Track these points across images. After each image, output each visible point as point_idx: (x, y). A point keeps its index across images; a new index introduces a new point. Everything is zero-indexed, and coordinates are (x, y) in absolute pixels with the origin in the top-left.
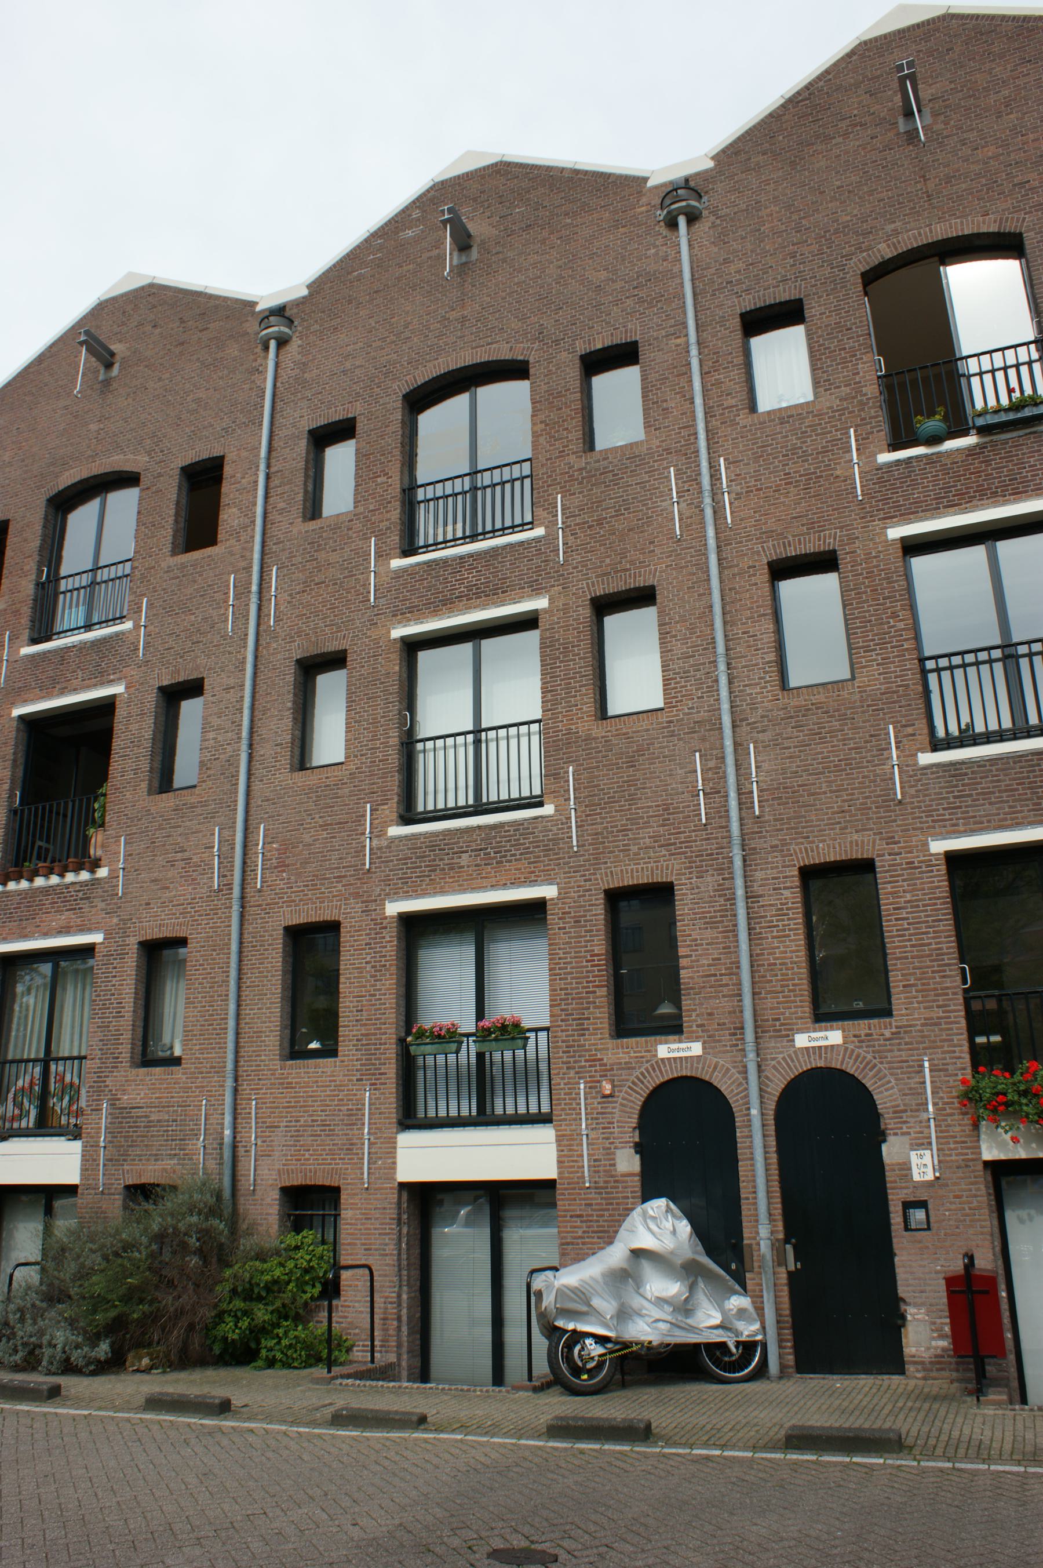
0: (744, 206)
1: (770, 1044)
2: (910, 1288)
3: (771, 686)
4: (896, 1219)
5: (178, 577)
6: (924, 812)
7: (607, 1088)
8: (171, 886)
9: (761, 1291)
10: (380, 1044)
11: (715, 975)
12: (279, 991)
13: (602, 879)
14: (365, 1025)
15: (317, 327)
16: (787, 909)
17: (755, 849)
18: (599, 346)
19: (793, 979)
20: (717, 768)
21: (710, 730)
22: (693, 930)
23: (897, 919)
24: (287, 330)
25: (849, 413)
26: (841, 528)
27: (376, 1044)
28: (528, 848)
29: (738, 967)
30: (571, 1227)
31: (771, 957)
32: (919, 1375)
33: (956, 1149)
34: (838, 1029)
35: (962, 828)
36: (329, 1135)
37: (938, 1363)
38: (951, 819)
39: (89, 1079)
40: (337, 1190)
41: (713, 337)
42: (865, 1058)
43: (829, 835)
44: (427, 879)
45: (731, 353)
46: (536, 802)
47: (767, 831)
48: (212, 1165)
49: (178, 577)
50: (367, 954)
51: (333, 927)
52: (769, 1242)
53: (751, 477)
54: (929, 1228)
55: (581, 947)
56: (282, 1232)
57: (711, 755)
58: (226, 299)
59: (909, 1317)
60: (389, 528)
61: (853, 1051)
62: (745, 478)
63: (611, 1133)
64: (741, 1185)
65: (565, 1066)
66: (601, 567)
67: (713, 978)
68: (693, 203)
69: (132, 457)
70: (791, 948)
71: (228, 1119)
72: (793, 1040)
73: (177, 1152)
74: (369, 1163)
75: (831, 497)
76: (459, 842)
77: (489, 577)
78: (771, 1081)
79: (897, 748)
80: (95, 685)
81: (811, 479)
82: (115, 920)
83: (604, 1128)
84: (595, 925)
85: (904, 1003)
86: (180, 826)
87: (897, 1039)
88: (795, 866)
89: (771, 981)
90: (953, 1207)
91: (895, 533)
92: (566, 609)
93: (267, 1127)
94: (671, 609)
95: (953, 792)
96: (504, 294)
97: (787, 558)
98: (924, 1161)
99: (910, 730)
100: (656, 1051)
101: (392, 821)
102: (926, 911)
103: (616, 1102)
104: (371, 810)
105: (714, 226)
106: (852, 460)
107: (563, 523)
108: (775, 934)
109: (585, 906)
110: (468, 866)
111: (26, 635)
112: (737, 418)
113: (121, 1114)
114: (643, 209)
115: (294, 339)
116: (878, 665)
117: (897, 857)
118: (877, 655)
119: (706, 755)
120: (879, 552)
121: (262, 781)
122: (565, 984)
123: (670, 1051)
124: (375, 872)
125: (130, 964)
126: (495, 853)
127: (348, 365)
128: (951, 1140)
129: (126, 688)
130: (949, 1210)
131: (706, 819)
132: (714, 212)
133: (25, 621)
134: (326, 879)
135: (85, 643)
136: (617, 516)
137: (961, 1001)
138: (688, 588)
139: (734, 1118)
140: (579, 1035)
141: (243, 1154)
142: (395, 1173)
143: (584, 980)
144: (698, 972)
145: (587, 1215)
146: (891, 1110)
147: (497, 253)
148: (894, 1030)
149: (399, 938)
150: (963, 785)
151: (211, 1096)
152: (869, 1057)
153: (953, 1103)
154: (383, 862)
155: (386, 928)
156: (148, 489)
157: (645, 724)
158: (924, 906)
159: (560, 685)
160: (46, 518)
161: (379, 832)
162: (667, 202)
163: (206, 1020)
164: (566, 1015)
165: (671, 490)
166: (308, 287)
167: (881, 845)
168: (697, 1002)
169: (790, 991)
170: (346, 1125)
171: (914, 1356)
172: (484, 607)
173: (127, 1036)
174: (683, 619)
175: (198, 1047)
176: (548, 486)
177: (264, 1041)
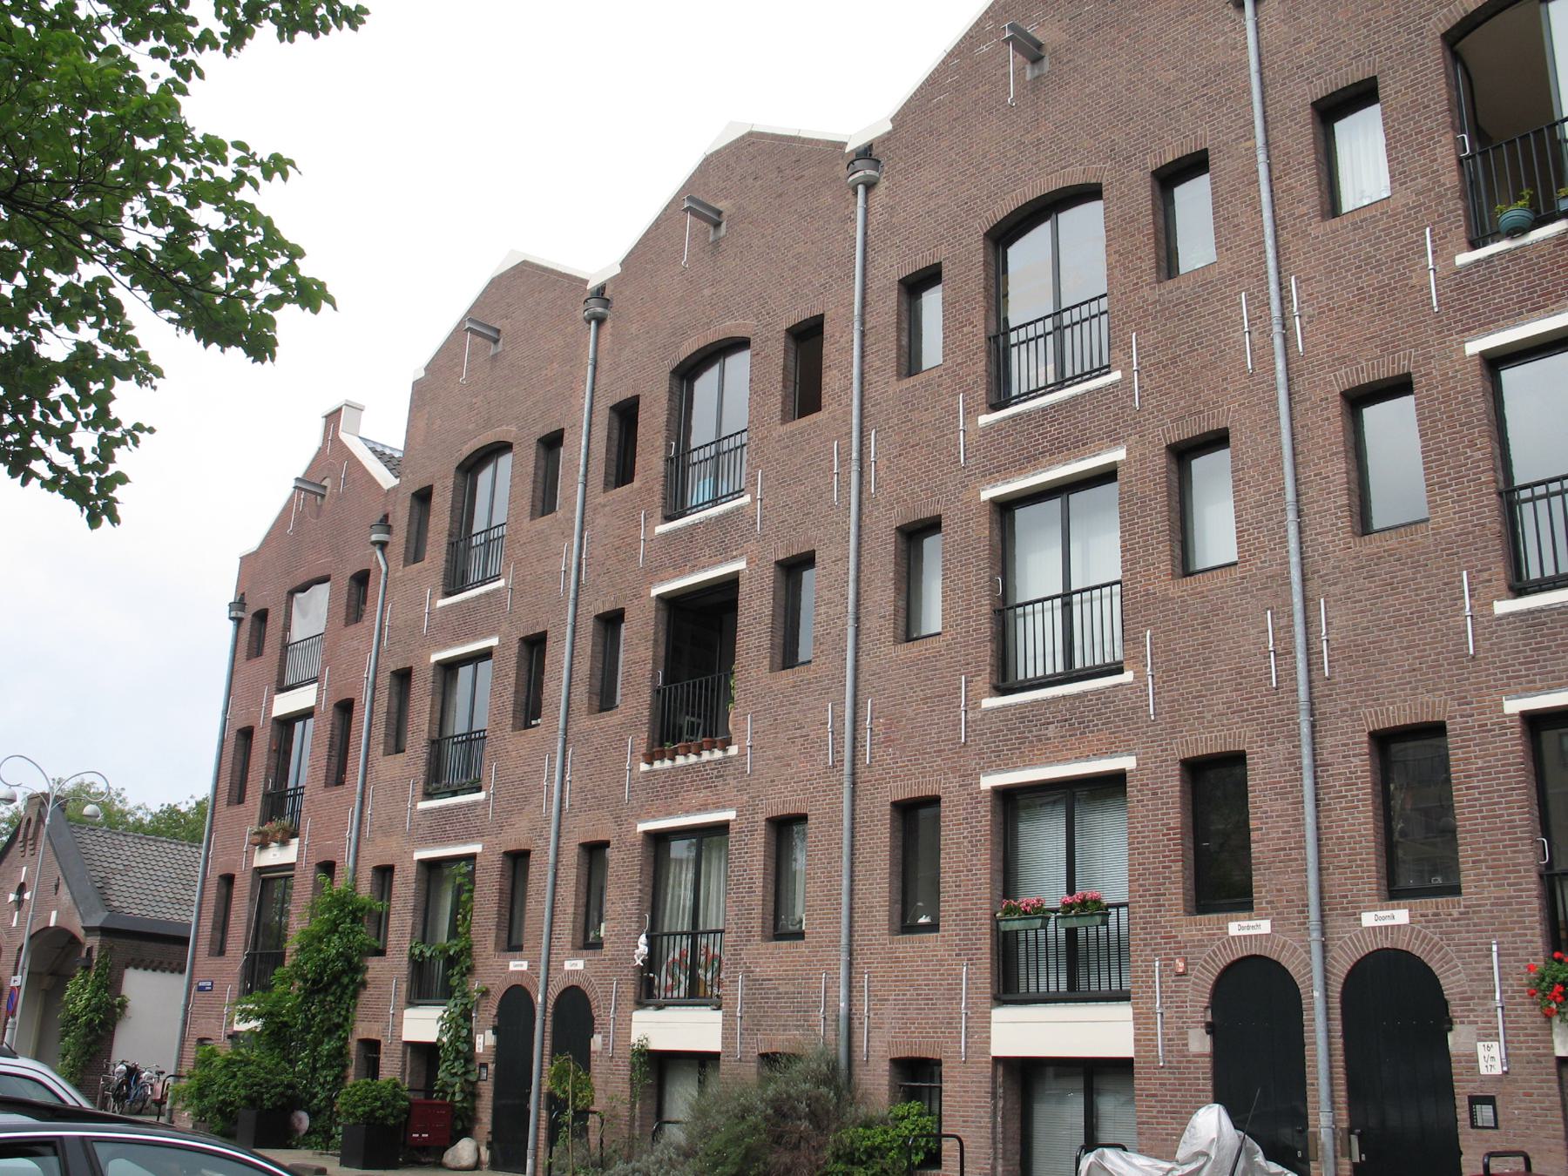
1: (1336, 922)
4: (1463, 1114)
7: (1180, 966)
15: (901, 164)
18: (1170, 159)
24: (873, 173)
39: (728, 950)
46: (1117, 669)
48: (831, 1035)
54: (1496, 1127)
56: (893, 1101)
70: (1358, 821)
71: (843, 992)
77: (1064, 429)
82: (745, 797)
97: (1361, 386)
99: (1485, 575)
111: (659, 513)
113: (753, 982)
123: (1241, 928)
126: (1077, 724)
133: (658, 499)
149: (993, 812)
152: (1436, 938)
157: (1393, 543)
160: (671, 391)
161: (973, 704)
167: (1452, 706)
172: (1066, 461)
173: (758, 910)
174: (1256, 463)
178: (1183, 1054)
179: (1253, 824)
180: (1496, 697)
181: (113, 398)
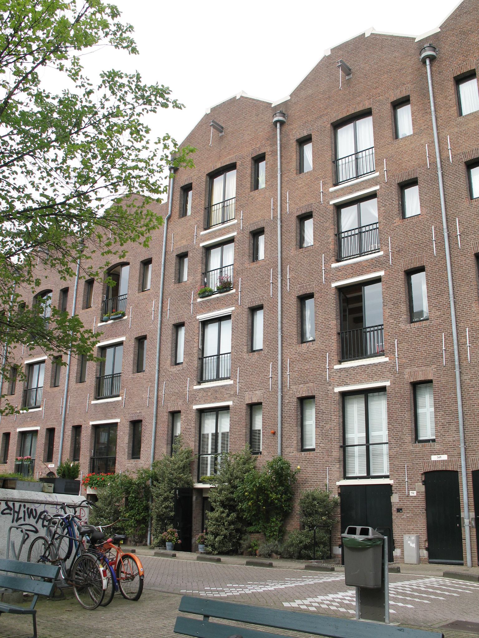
181: (141, 77)
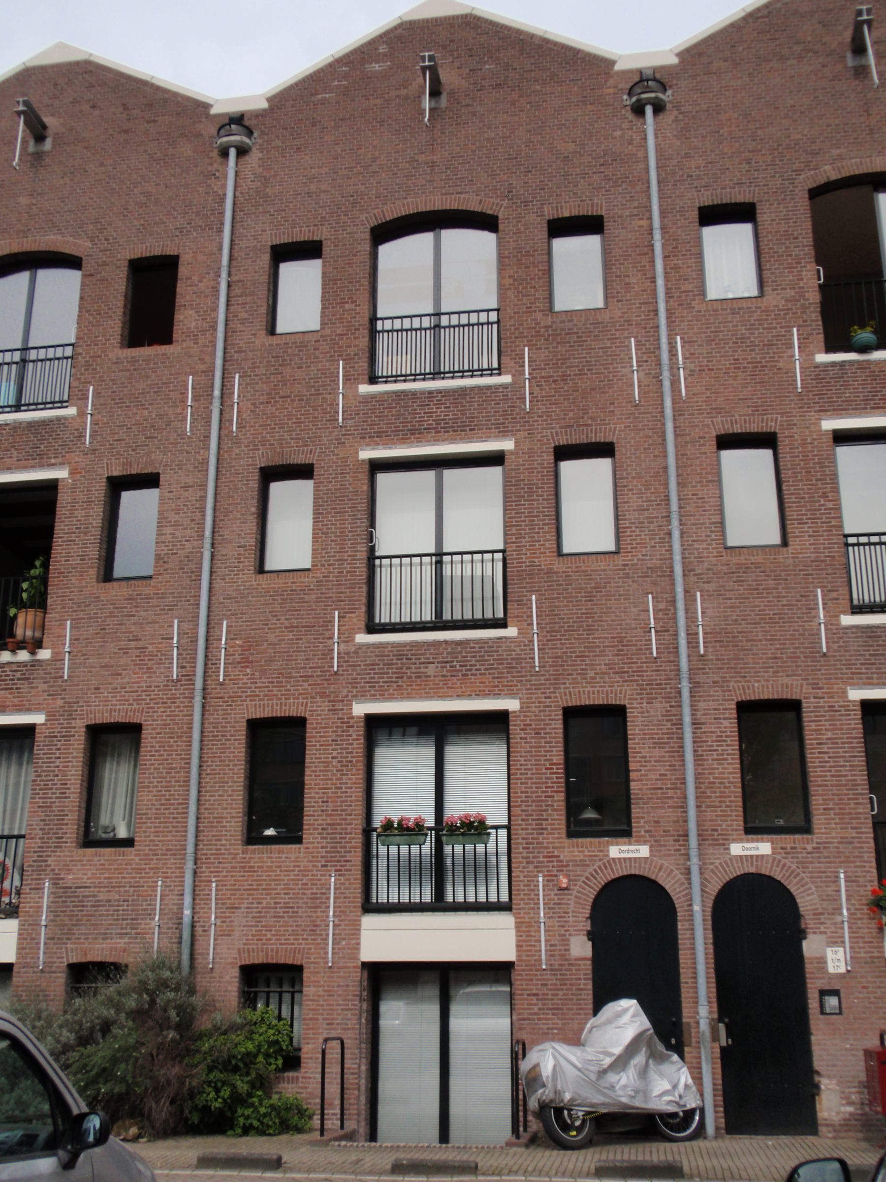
0: (705, 107)
2: (825, 1063)
3: (717, 544)
4: (813, 1004)
5: (129, 370)
6: (844, 665)
7: (564, 882)
8: (124, 672)
9: (700, 1063)
10: (346, 834)
11: (662, 789)
12: (242, 779)
13: (561, 697)
14: (331, 815)
15: (278, 143)
16: (727, 736)
17: (699, 683)
18: (566, 214)
19: (730, 797)
20: (667, 610)
21: (661, 576)
22: (643, 748)
23: (819, 753)
24: (246, 140)
25: (793, 313)
26: (782, 414)
27: (341, 833)
28: (493, 664)
29: (684, 783)
30: (528, 1004)
31: (711, 777)
32: (830, 1135)
33: (864, 948)
34: (767, 841)
35: (875, 681)
36: (292, 917)
37: (846, 1125)
38: (867, 673)
40: (299, 969)
41: (673, 224)
42: (790, 867)
43: (763, 676)
44: (395, 685)
45: (689, 242)
47: (710, 669)
49: (129, 370)
50: (333, 750)
51: (299, 723)
52: (707, 1021)
53: (704, 358)
54: (840, 1013)
55: (541, 756)
57: (662, 598)
58: (176, 95)
59: (823, 1087)
60: (358, 354)
61: (780, 861)
62: (699, 358)
63: (566, 922)
64: (682, 971)
65: (524, 861)
66: (564, 419)
67: (660, 791)
68: (661, 95)
69: (71, 239)
70: (728, 769)
71: (188, 899)
72: (728, 849)
73: (129, 931)
74: (333, 944)
75: (774, 385)
76: (425, 654)
78: (709, 882)
79: (824, 608)
80: (33, 467)
81: (757, 367)
82: (60, 702)
83: (559, 917)
84: (554, 738)
85: (824, 824)
86: (134, 616)
87: (817, 852)
88: (733, 700)
89: (710, 797)
90: (861, 996)
91: (830, 424)
92: (531, 453)
93: (227, 908)
94: (629, 466)
95: (869, 650)
96: (474, 147)
97: (750, 433)
98: (838, 957)
100: (608, 851)
101: (360, 628)
102: (844, 748)
103: (571, 895)
104: (339, 617)
105: (676, 120)
106: (793, 356)
107: (529, 374)
108: (715, 757)
109: (545, 720)
110: (435, 676)
112: (693, 303)
113: (64, 894)
114: (611, 90)
115: (254, 150)
116: (809, 536)
117: (821, 700)
118: (809, 527)
119: (657, 598)
120: (814, 439)
121: (224, 579)
122: (526, 788)
123: (621, 851)
124: (342, 675)
125: (78, 745)
127: (313, 187)
128: (861, 940)
129: (70, 473)
130: (858, 998)
131: (657, 653)
132: (677, 107)
134: (291, 677)
135: (21, 423)
136: (580, 375)
137: (871, 825)
138: (645, 449)
139: (676, 912)
140: (538, 834)
141: (201, 933)
142: (359, 953)
143: (544, 786)
144: (647, 785)
145: (543, 994)
146: (812, 912)
147: (467, 105)
148: (815, 845)
150: (878, 646)
151: (167, 877)
152: (794, 866)
153: (863, 909)
154: (350, 666)
155: (353, 727)
156: (91, 275)
157: (602, 566)
158: (843, 743)
159: (525, 521)
161: (347, 638)
162: (638, 90)
163: (162, 804)
164: (526, 815)
165: (631, 358)
166: (269, 100)
167: (807, 689)
168: (645, 810)
169: (727, 806)
170: (311, 907)
171: (826, 1120)
172: (453, 440)
175: (153, 830)
176: (516, 338)
177: (225, 827)
178: (564, 955)
179: (632, 766)
180: (843, 687)
